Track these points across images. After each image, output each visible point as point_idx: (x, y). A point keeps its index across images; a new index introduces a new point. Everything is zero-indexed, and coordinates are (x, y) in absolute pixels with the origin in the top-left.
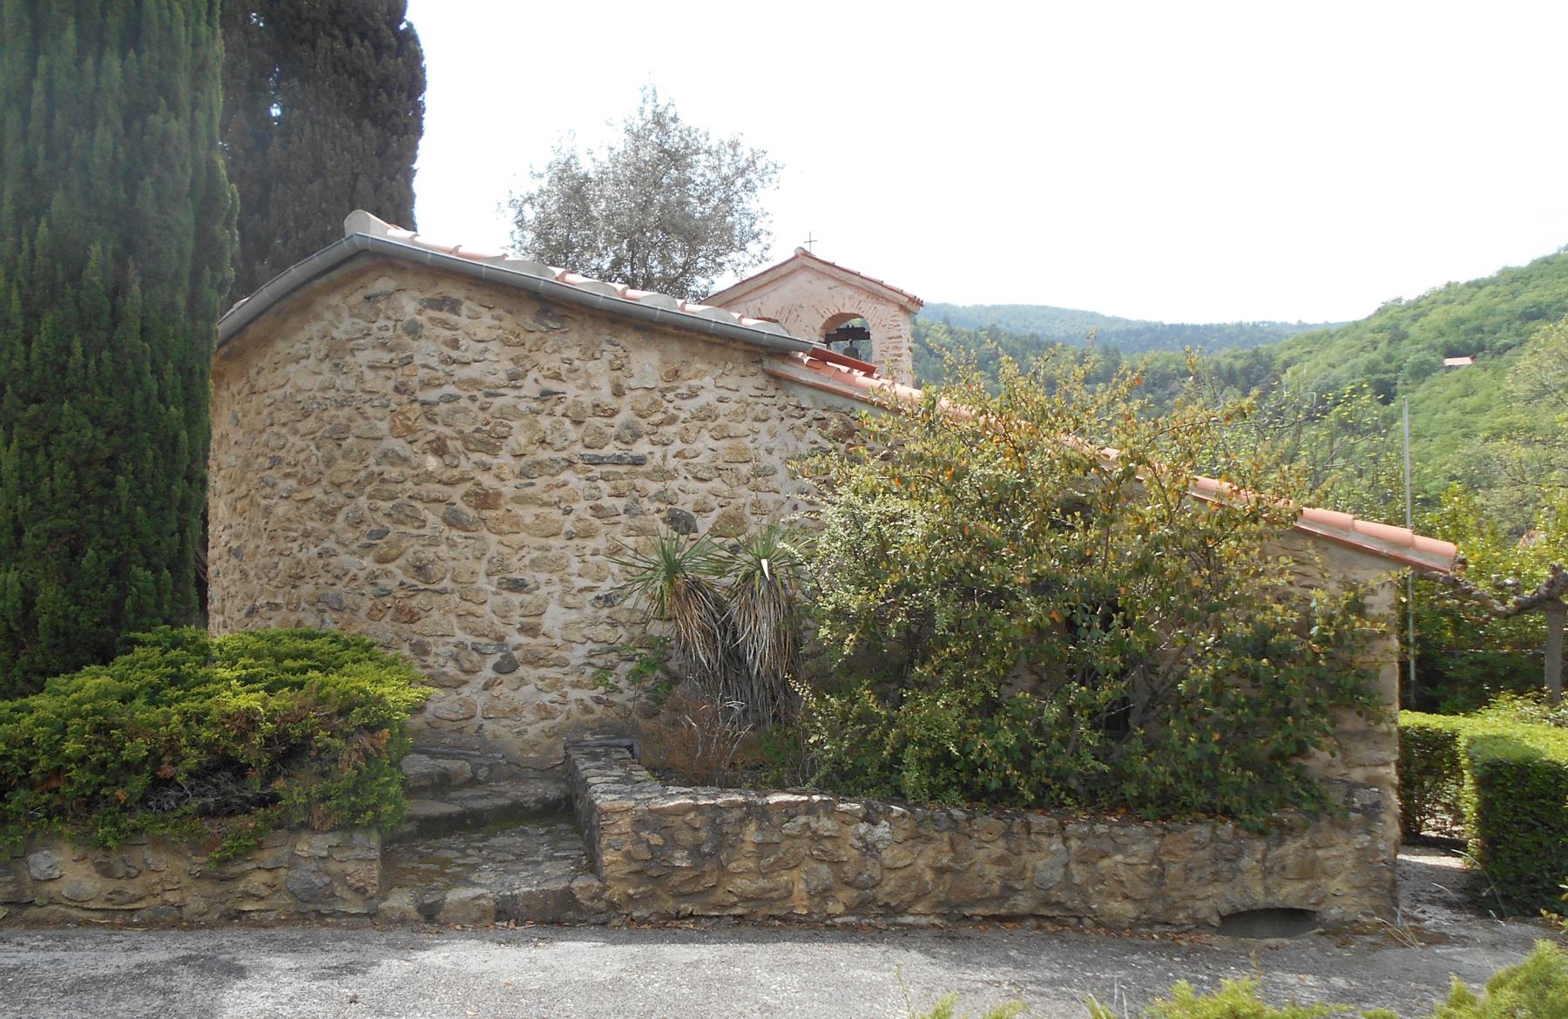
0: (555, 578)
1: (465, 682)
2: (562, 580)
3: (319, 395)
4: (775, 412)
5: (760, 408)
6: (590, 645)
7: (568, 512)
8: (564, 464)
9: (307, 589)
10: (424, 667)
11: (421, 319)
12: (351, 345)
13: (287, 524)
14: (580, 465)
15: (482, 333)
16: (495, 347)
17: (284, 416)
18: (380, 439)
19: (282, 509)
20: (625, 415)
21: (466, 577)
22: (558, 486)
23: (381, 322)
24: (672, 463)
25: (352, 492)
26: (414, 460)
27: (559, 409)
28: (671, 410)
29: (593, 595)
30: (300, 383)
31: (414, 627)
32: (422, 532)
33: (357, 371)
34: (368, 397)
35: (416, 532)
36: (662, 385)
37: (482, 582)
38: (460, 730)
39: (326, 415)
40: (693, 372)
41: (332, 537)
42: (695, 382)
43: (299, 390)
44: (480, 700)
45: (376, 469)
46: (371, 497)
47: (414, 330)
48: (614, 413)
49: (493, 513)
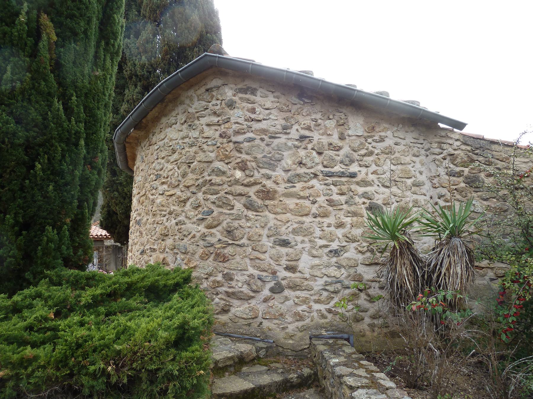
0: (306, 239)
1: (253, 297)
3: (180, 142)
4: (423, 152)
5: (416, 149)
6: (325, 279)
7: (314, 203)
8: (312, 175)
9: (169, 242)
10: (230, 287)
11: (236, 99)
12: (198, 114)
13: (161, 208)
14: (321, 177)
15: (268, 105)
17: (163, 154)
18: (211, 162)
19: (159, 200)
20: (346, 150)
21: (256, 237)
23: (214, 102)
24: (371, 177)
25: (195, 191)
26: (229, 173)
27: (310, 146)
28: (371, 148)
29: (327, 250)
30: (171, 136)
31: (226, 265)
32: (232, 212)
34: (206, 140)
35: (228, 212)
36: (366, 134)
38: (249, 325)
39: (184, 152)
40: (382, 128)
41: (184, 214)
42: (383, 134)
43: (171, 140)
44: (262, 308)
45: (208, 178)
46: (204, 193)
47: (231, 105)
48: (340, 148)
49: (272, 202)
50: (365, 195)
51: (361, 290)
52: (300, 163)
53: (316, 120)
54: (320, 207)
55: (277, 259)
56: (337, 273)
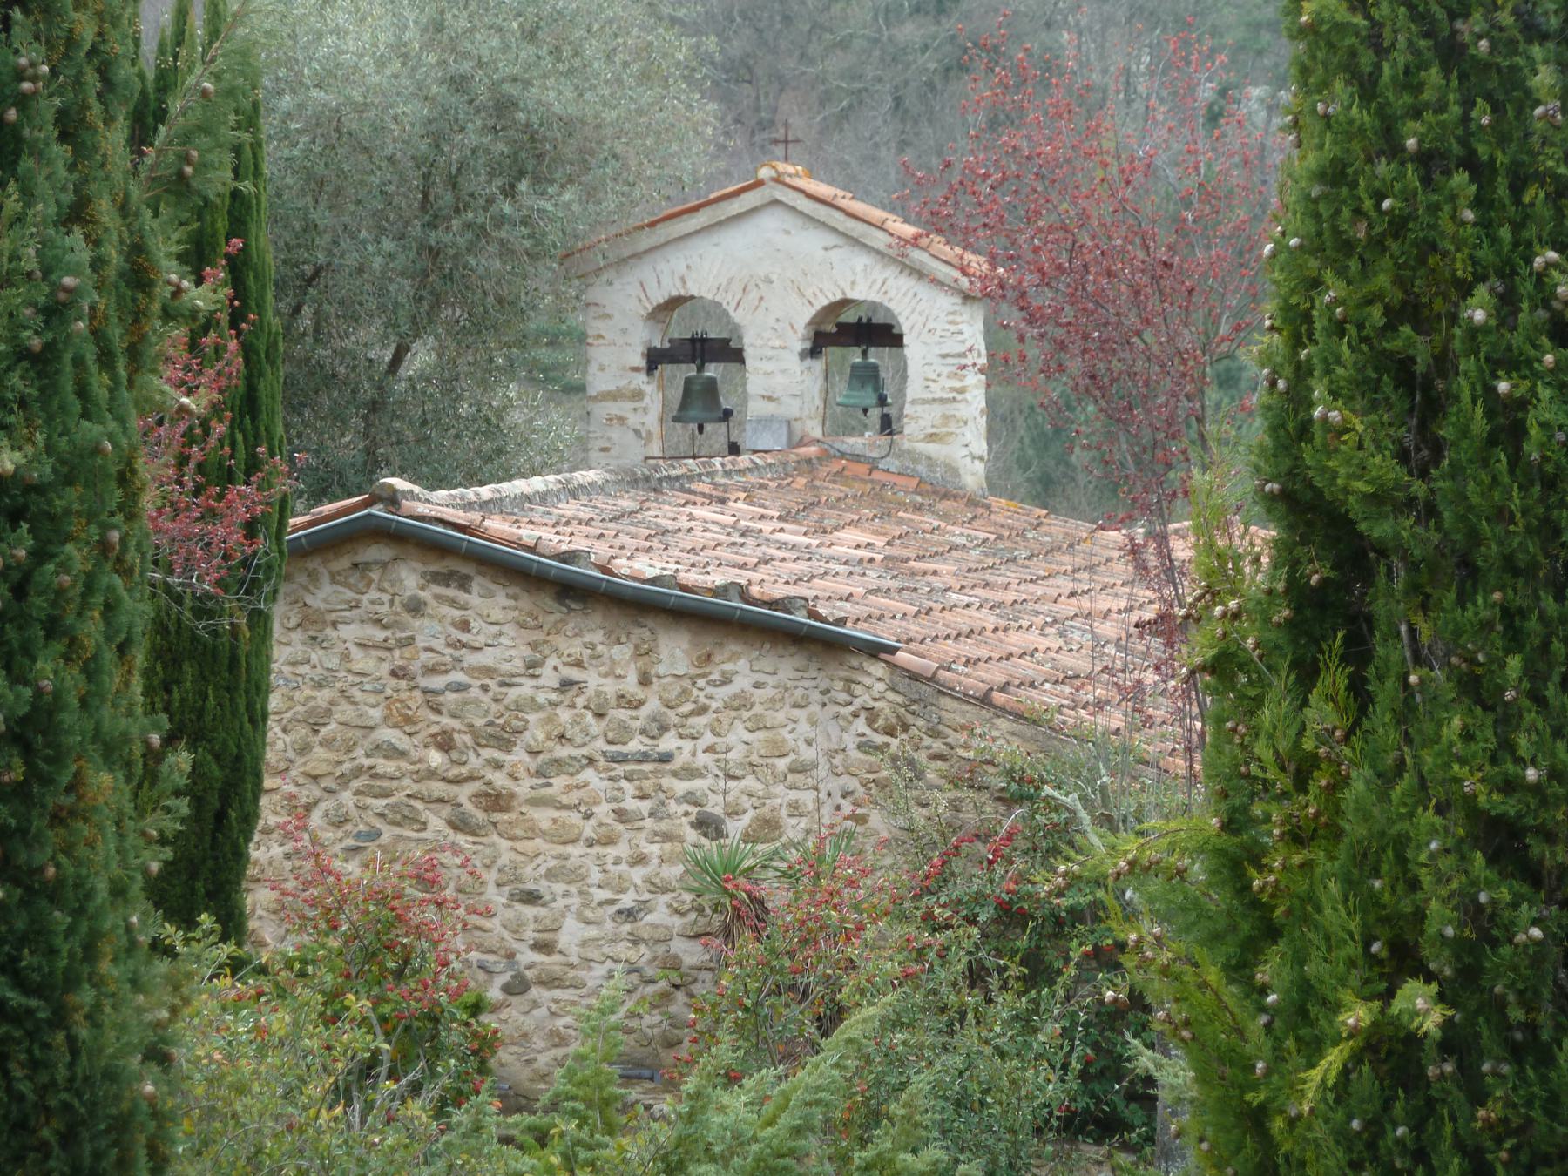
0: (573, 889)
2: (580, 892)
4: (816, 696)
5: (799, 693)
7: (588, 816)
12: (333, 616)
14: (602, 763)
15: (497, 615)
16: (510, 630)
20: (653, 705)
22: (578, 787)
24: (703, 759)
27: (580, 701)
28: (703, 700)
29: (613, 909)
33: (340, 647)
34: (357, 679)
37: (491, 889)
42: (728, 667)
45: (367, 762)
47: (415, 608)
48: (640, 704)
49: (506, 817)
50: (690, 798)
51: (677, 987)
52: (562, 737)
53: (593, 646)
54: (601, 825)
55: (516, 929)
56: (632, 955)
